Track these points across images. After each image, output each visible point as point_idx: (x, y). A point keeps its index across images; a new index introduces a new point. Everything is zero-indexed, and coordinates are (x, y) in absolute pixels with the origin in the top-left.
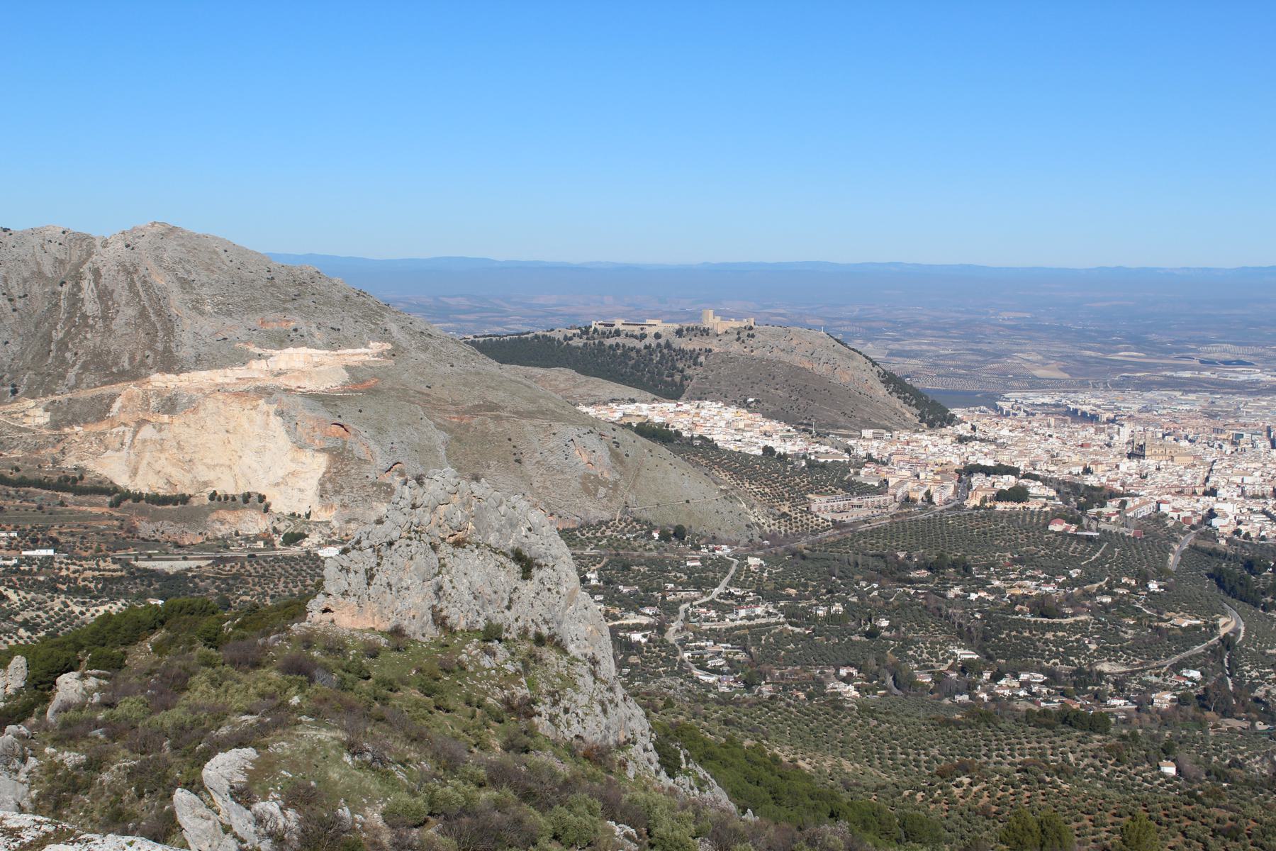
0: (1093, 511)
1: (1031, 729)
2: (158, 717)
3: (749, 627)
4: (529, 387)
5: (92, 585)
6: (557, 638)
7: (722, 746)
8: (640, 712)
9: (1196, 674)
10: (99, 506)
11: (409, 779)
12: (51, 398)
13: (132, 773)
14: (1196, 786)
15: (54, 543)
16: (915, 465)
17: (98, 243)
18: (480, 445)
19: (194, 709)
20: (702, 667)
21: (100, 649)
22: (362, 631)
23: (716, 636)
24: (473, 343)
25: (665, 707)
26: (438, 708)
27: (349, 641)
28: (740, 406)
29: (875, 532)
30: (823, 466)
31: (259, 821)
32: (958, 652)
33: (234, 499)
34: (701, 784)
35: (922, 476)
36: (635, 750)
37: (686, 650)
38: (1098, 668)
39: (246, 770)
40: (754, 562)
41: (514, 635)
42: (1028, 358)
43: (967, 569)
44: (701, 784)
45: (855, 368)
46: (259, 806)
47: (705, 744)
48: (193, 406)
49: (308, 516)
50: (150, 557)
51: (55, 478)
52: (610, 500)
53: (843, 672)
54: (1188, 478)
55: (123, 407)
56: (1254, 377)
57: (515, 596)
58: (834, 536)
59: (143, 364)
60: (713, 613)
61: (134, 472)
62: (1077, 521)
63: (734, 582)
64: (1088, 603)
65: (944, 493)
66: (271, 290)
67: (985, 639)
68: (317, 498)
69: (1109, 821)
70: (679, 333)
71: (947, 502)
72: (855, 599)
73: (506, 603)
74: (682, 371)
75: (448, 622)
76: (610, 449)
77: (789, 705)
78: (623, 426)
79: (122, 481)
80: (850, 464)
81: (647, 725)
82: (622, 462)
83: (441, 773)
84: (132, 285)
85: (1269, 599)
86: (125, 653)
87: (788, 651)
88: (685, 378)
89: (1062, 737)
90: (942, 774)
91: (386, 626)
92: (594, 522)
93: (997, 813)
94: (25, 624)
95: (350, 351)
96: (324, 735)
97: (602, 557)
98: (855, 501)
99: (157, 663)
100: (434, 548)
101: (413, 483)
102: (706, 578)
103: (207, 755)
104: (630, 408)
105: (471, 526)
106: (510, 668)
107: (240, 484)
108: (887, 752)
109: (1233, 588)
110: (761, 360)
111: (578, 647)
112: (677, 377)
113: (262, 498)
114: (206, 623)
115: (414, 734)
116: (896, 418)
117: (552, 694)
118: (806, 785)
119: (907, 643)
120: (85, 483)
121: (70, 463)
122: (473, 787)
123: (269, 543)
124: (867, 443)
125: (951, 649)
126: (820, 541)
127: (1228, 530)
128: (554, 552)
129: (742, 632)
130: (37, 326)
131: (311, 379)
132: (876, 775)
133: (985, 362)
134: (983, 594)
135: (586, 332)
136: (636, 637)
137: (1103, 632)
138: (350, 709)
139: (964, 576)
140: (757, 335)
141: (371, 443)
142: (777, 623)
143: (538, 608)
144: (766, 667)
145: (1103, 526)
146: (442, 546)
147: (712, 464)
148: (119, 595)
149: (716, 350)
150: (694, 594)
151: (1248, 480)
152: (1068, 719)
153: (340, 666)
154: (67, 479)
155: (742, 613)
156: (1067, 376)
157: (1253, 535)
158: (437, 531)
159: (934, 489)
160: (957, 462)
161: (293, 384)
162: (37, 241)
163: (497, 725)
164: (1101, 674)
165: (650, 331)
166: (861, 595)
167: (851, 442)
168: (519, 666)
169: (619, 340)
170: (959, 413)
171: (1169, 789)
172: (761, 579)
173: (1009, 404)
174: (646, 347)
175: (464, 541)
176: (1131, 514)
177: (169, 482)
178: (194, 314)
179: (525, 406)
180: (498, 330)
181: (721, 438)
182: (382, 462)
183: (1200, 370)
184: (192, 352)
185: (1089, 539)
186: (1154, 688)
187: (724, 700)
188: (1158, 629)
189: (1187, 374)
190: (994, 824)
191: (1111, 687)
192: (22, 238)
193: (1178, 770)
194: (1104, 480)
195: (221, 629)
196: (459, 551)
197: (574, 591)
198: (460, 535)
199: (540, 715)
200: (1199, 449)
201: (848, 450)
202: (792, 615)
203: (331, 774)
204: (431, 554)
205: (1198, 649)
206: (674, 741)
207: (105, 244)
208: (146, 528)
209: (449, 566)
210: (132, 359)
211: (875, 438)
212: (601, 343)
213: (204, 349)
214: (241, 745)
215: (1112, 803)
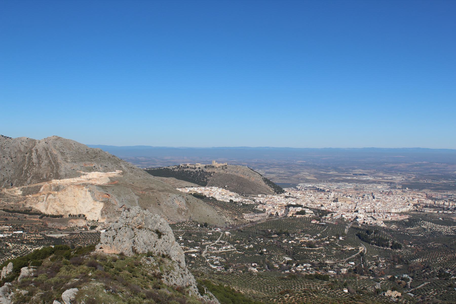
0: (324, 217)
1: (307, 280)
2: (50, 280)
3: (226, 252)
5: (34, 242)
6: (169, 256)
7: (218, 286)
8: (193, 277)
9: (353, 263)
10: (36, 218)
11: (123, 297)
12: (23, 187)
13: (42, 296)
15: (23, 229)
16: (274, 204)
17: (37, 142)
18: (148, 200)
19: (60, 277)
20: (213, 264)
21: (35, 260)
22: (112, 254)
23: (217, 255)
24: (146, 170)
25: (201, 275)
26: (134, 276)
28: (223, 188)
29: (262, 224)
30: (247, 205)
32: (286, 258)
33: (76, 216)
34: (211, 298)
35: (275, 208)
37: (208, 259)
38: (326, 262)
39: (75, 295)
41: (156, 255)
42: (305, 174)
43: (288, 234)
44: (211, 298)
47: (213, 286)
48: (64, 189)
49: (98, 221)
50: (51, 233)
51: (23, 210)
53: (253, 265)
54: (350, 207)
55: (44, 189)
56: (368, 179)
57: (156, 243)
59: (50, 177)
60: (215, 248)
61: (47, 208)
62: (319, 220)
64: (322, 244)
65: (281, 213)
67: (294, 254)
68: (100, 216)
70: (206, 167)
71: (282, 215)
72: (256, 243)
73: (154, 245)
75: (137, 251)
77: (237, 274)
79: (43, 211)
81: (195, 280)
82: (189, 205)
83: (133, 295)
84: (47, 154)
85: (373, 241)
86: (42, 261)
87: (237, 259)
88: (207, 180)
90: (281, 294)
91: (119, 252)
92: (181, 222)
94: (14, 253)
95: (110, 173)
96: (98, 284)
98: (256, 215)
99: (51, 264)
100: (133, 230)
101: (126, 210)
103: (64, 290)
104: (191, 189)
105: (143, 223)
106: (155, 264)
107: (78, 212)
108: (266, 287)
109: (363, 239)
110: (229, 175)
112: (205, 180)
113: (84, 216)
114: (66, 252)
115: (125, 284)
116: (268, 191)
117: (167, 272)
119: (271, 256)
120: (32, 212)
121: (28, 206)
122: (142, 299)
123: (86, 229)
124: (260, 198)
125: (284, 257)
127: (361, 222)
128: (167, 230)
130: (19, 166)
132: (263, 294)
133: (293, 175)
134: (293, 241)
135: (179, 167)
136: (193, 255)
137: (327, 252)
138: (107, 277)
141: (116, 199)
143: (163, 247)
145: (326, 221)
146: (135, 229)
147: (215, 205)
148: (42, 244)
149: (216, 172)
151: (367, 208)
152: (317, 277)
153: (105, 264)
154: (27, 210)
155: (224, 248)
157: (368, 223)
159: (278, 211)
160: (285, 204)
161: (94, 182)
162: (19, 141)
163: (151, 281)
164: (326, 264)
165: (197, 167)
166: (258, 242)
167: (255, 198)
168: (157, 264)
169: (188, 169)
170: (285, 189)
175: (141, 227)
177: (57, 211)
178: (65, 162)
180: (154, 166)
181: (218, 197)
182: (119, 205)
183: (353, 177)
184: (64, 173)
185: (323, 225)
186: (341, 267)
187: (219, 273)
188: (342, 250)
189: (349, 178)
191: (329, 267)
192: (15, 141)
193: (348, 291)
194: (327, 208)
195: (70, 254)
196: (140, 230)
197: (173, 242)
198: (140, 226)
200: (353, 199)
201: (254, 200)
202: (239, 248)
204: (132, 231)
205: (354, 256)
206: (203, 285)
207: (39, 142)
208: (50, 225)
210: (47, 175)
212: (183, 170)
213: (68, 172)
214: (73, 287)
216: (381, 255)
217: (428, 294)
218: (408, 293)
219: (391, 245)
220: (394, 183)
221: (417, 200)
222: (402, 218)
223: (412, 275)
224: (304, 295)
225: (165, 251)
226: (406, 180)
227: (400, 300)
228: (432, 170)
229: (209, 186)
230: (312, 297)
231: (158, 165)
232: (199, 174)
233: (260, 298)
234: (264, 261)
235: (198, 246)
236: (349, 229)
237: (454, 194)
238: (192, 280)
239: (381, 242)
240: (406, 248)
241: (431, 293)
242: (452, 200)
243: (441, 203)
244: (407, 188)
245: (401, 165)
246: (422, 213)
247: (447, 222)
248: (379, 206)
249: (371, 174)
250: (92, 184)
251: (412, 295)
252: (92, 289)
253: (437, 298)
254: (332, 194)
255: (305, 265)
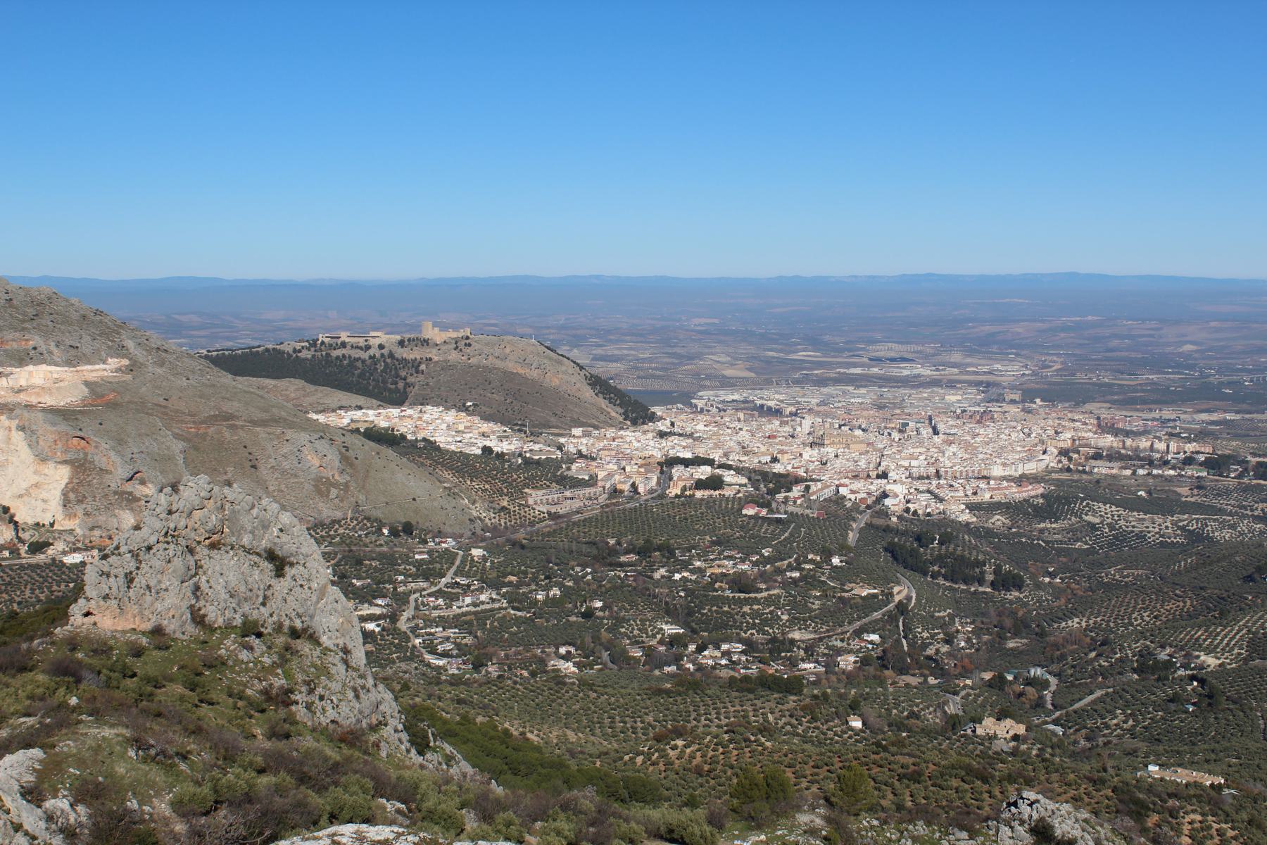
0: (780, 496)
1: (735, 694)
3: (475, 613)
4: (262, 397)
6: (311, 631)
7: (458, 723)
8: (389, 696)
11: (192, 770)
14: (880, 737)
16: (621, 458)
18: (217, 449)
20: (433, 651)
22: (124, 632)
23: (444, 622)
24: (206, 357)
26: (201, 701)
27: (112, 642)
28: (459, 410)
30: (538, 462)
31: (50, 818)
32: (665, 627)
34: (449, 759)
36: (387, 732)
37: (417, 636)
38: (790, 636)
39: (34, 770)
40: (477, 552)
41: (269, 630)
42: (718, 359)
43: (672, 554)
45: (564, 373)
46: (49, 804)
49: (52, 525)
52: (342, 501)
53: (562, 650)
56: (916, 372)
57: (269, 593)
58: (549, 526)
60: (440, 601)
62: (767, 505)
63: (459, 572)
64: (779, 579)
66: (9, 310)
68: (61, 508)
69: (808, 772)
71: (651, 491)
72: (571, 584)
73: (261, 599)
74: (405, 379)
76: (340, 453)
77: (515, 683)
78: (352, 431)
80: (562, 461)
82: (351, 465)
85: (936, 568)
88: (407, 385)
89: (763, 699)
90: (658, 739)
91: (148, 626)
93: (709, 771)
95: (89, 367)
96: (107, 732)
97: (336, 554)
98: (568, 494)
102: (434, 569)
104: (358, 415)
106: (267, 660)
110: (479, 367)
111: (330, 638)
112: (401, 385)
115: (192, 727)
116: (602, 417)
117: (307, 683)
118: (537, 755)
119: (619, 621)
122: (254, 774)
123: (15, 552)
124: (577, 441)
126: (537, 532)
128: (304, 550)
129: (468, 618)
131: (51, 394)
133: (680, 364)
134: (686, 574)
137: (794, 605)
139: (668, 558)
140: (474, 344)
141: (112, 454)
142: (500, 608)
144: (490, 649)
145: (790, 509)
146: (198, 549)
149: (436, 359)
150: (424, 585)
151: (914, 463)
155: (468, 600)
156: (753, 375)
157: (920, 512)
158: (193, 535)
160: (659, 456)
164: (792, 642)
165: (375, 342)
166: (577, 580)
167: (562, 440)
169: (344, 351)
170: (658, 410)
171: (857, 741)
172: (484, 568)
173: (703, 402)
174: (371, 357)
175: (219, 542)
176: (814, 497)
179: (259, 415)
180: (229, 344)
181: (443, 440)
182: (122, 472)
183: (870, 367)
185: (779, 521)
186: (839, 652)
187: (456, 681)
189: (858, 371)
190: (708, 782)
191: (802, 652)
193: (864, 724)
194: (789, 468)
196: (214, 553)
197: (325, 587)
199: (297, 703)
201: (560, 447)
202: (516, 600)
203: (117, 769)
209: (205, 567)
211: (584, 436)
214: (28, 746)
215: (810, 757)
216: (959, 612)
217: (1107, 727)
218: (1047, 723)
219: (990, 577)
220: (997, 385)
221: (1068, 435)
222: (1025, 495)
223: (1054, 668)
224: (730, 741)
225: (299, 616)
226: (1034, 374)
227: (1024, 747)
228: (1115, 343)
229: (413, 405)
230: (754, 746)
231: (244, 341)
232: (381, 367)
233: (591, 756)
234: (596, 639)
235: (384, 596)
236: (861, 531)
237: (1182, 417)
238: (389, 705)
239: (961, 570)
240: (1038, 586)
241: (1115, 721)
242: (1177, 435)
243: (1144, 443)
244: (1038, 400)
245: (1019, 329)
246: (1084, 476)
247: (1161, 503)
248: (951, 459)
249: (926, 359)
250: (29, 407)
251: (1059, 730)
252: (90, 748)
253: (1133, 736)
254: (807, 423)
255: (725, 647)
